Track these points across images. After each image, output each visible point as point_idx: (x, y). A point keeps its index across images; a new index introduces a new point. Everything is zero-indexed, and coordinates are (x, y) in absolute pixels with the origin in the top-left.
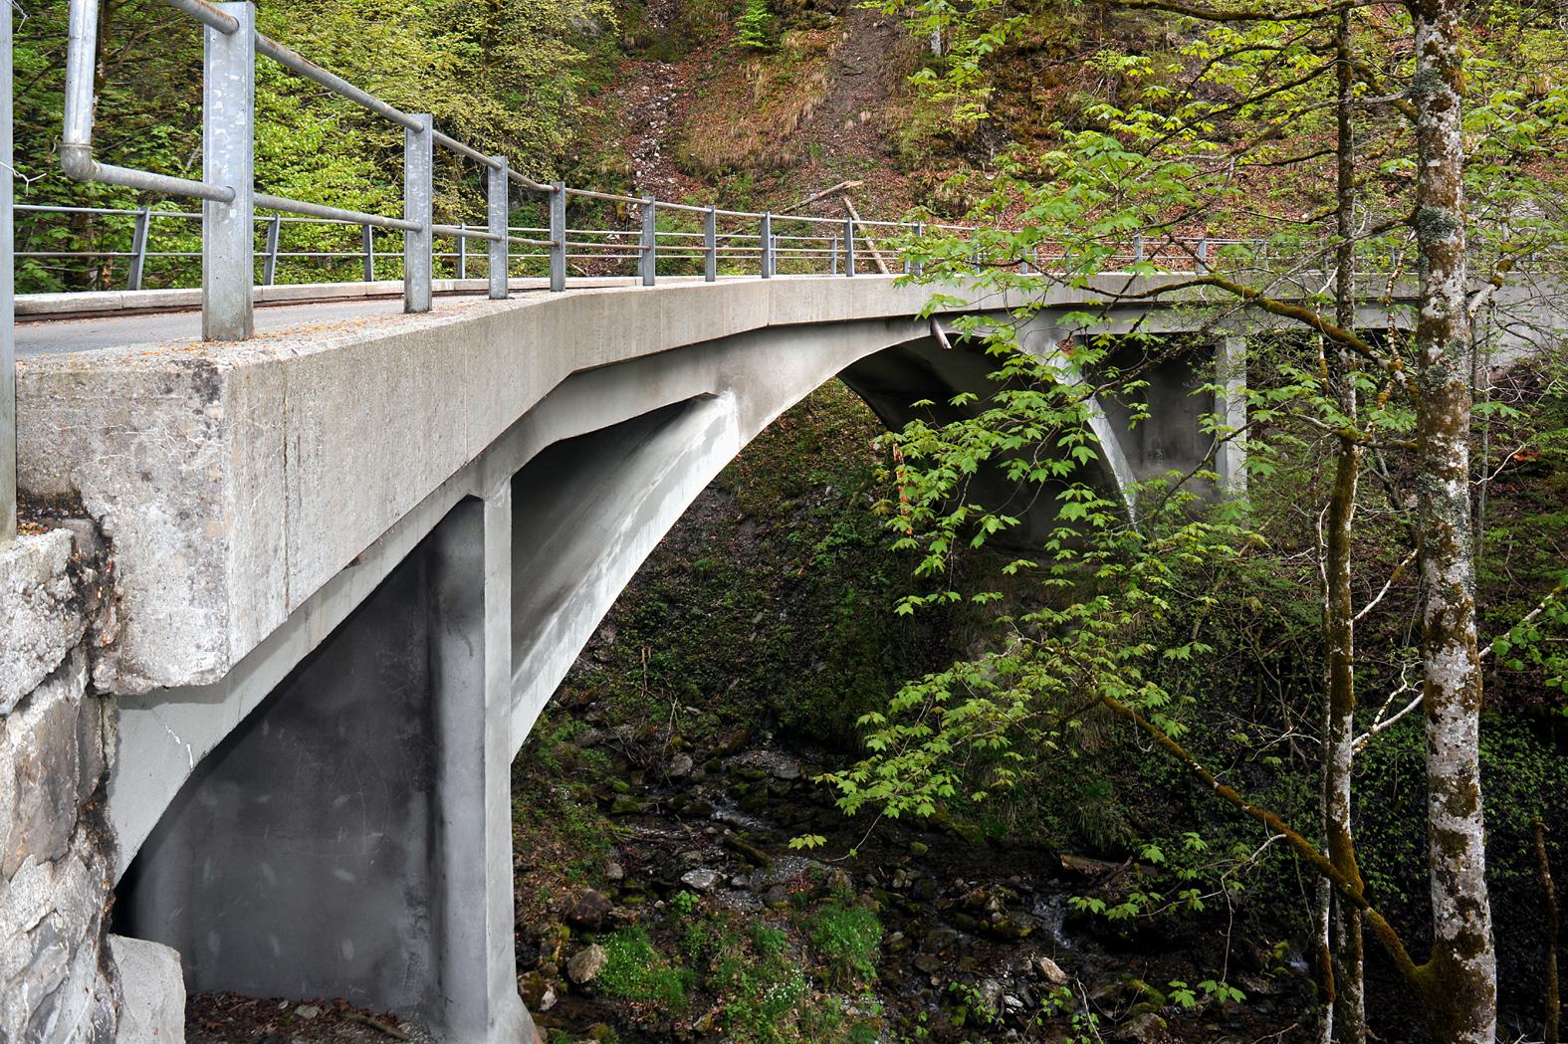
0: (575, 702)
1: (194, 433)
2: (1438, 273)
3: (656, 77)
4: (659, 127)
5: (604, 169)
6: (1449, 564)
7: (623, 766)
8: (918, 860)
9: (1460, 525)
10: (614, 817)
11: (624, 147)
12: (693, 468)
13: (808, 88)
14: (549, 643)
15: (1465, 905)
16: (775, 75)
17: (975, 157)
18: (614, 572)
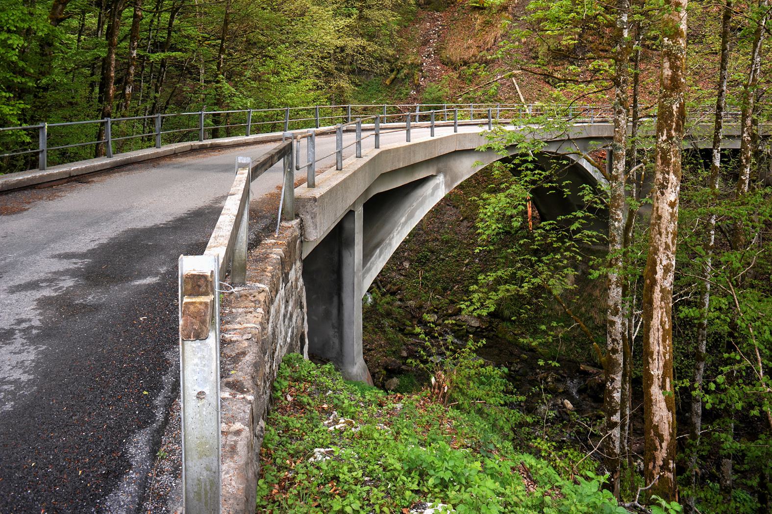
0: (392, 290)
1: (313, 207)
2: (616, 162)
3: (433, 19)
4: (434, 43)
5: (409, 62)
6: (614, 245)
7: (410, 316)
8: (523, 361)
9: (618, 234)
10: (405, 335)
11: (418, 51)
12: (427, 201)
13: (499, 26)
14: (376, 258)
15: (614, 340)
16: (484, 19)
17: (572, 60)
18: (398, 236)
